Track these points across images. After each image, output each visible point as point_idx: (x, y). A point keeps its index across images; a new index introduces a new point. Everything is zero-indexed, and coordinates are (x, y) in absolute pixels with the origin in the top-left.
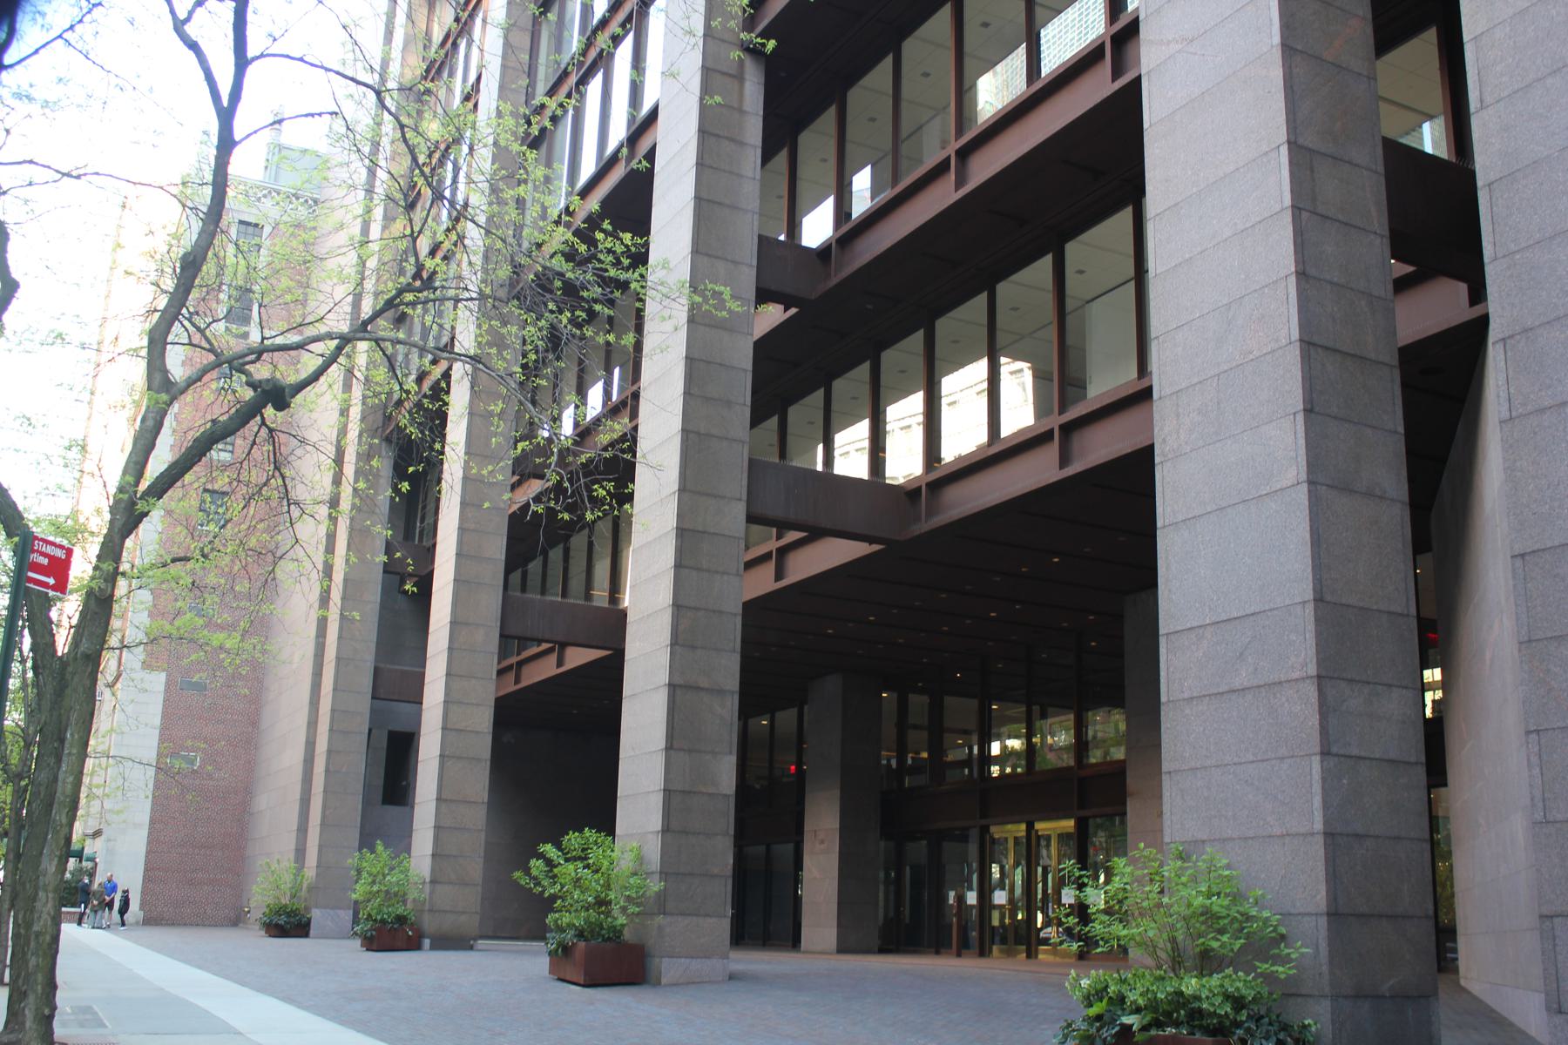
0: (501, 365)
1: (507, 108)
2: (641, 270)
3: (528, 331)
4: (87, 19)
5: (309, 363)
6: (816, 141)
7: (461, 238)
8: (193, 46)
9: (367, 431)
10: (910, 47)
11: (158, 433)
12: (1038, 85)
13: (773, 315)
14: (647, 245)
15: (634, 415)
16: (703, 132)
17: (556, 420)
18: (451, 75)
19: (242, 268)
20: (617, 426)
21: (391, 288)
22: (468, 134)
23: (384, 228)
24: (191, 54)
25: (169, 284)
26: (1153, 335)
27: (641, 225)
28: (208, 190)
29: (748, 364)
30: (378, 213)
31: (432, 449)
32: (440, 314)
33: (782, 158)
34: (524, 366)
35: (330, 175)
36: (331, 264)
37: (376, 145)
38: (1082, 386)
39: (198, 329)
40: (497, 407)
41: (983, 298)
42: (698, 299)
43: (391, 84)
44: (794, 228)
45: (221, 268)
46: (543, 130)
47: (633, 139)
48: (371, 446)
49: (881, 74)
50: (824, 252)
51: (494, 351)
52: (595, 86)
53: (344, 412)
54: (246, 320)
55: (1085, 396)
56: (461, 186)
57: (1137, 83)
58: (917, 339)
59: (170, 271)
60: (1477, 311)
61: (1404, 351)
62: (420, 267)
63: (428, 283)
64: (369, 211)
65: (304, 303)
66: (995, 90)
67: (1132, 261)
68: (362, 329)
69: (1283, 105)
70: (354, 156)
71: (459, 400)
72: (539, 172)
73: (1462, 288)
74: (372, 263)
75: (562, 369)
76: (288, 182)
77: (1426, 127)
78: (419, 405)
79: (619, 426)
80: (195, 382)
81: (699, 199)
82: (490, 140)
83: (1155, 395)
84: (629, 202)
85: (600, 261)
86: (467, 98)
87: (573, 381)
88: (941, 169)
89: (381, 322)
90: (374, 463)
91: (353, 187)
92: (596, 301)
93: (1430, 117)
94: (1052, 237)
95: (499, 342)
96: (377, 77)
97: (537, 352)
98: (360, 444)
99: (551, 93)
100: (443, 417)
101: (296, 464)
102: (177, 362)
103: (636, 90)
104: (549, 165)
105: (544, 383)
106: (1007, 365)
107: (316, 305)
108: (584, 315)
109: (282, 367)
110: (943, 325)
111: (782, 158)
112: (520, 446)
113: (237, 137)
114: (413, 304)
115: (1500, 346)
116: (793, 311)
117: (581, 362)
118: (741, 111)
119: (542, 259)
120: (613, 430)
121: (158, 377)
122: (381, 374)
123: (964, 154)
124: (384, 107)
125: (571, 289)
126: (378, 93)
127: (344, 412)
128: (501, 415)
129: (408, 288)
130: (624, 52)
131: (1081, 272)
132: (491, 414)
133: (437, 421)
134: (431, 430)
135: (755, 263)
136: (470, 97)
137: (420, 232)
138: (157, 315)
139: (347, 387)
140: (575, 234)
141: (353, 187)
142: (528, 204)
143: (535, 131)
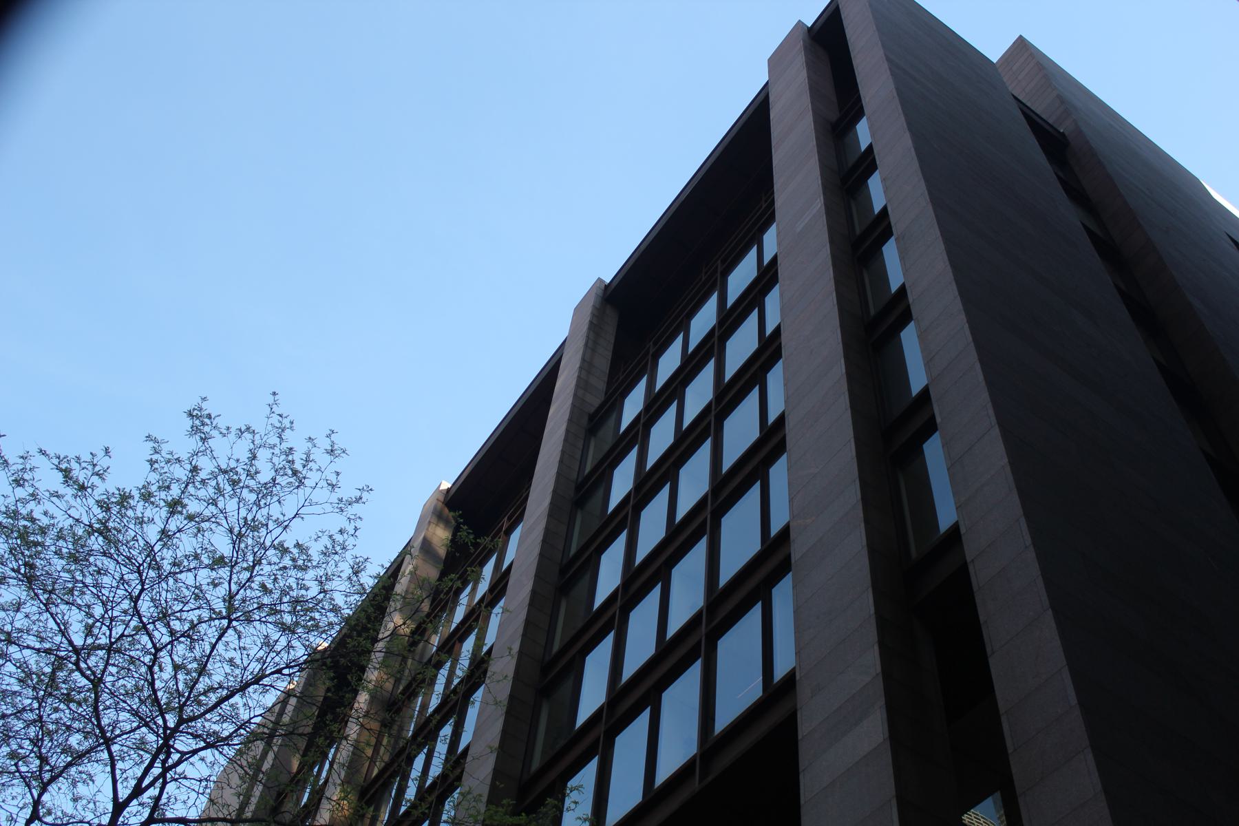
130: (447, 730)
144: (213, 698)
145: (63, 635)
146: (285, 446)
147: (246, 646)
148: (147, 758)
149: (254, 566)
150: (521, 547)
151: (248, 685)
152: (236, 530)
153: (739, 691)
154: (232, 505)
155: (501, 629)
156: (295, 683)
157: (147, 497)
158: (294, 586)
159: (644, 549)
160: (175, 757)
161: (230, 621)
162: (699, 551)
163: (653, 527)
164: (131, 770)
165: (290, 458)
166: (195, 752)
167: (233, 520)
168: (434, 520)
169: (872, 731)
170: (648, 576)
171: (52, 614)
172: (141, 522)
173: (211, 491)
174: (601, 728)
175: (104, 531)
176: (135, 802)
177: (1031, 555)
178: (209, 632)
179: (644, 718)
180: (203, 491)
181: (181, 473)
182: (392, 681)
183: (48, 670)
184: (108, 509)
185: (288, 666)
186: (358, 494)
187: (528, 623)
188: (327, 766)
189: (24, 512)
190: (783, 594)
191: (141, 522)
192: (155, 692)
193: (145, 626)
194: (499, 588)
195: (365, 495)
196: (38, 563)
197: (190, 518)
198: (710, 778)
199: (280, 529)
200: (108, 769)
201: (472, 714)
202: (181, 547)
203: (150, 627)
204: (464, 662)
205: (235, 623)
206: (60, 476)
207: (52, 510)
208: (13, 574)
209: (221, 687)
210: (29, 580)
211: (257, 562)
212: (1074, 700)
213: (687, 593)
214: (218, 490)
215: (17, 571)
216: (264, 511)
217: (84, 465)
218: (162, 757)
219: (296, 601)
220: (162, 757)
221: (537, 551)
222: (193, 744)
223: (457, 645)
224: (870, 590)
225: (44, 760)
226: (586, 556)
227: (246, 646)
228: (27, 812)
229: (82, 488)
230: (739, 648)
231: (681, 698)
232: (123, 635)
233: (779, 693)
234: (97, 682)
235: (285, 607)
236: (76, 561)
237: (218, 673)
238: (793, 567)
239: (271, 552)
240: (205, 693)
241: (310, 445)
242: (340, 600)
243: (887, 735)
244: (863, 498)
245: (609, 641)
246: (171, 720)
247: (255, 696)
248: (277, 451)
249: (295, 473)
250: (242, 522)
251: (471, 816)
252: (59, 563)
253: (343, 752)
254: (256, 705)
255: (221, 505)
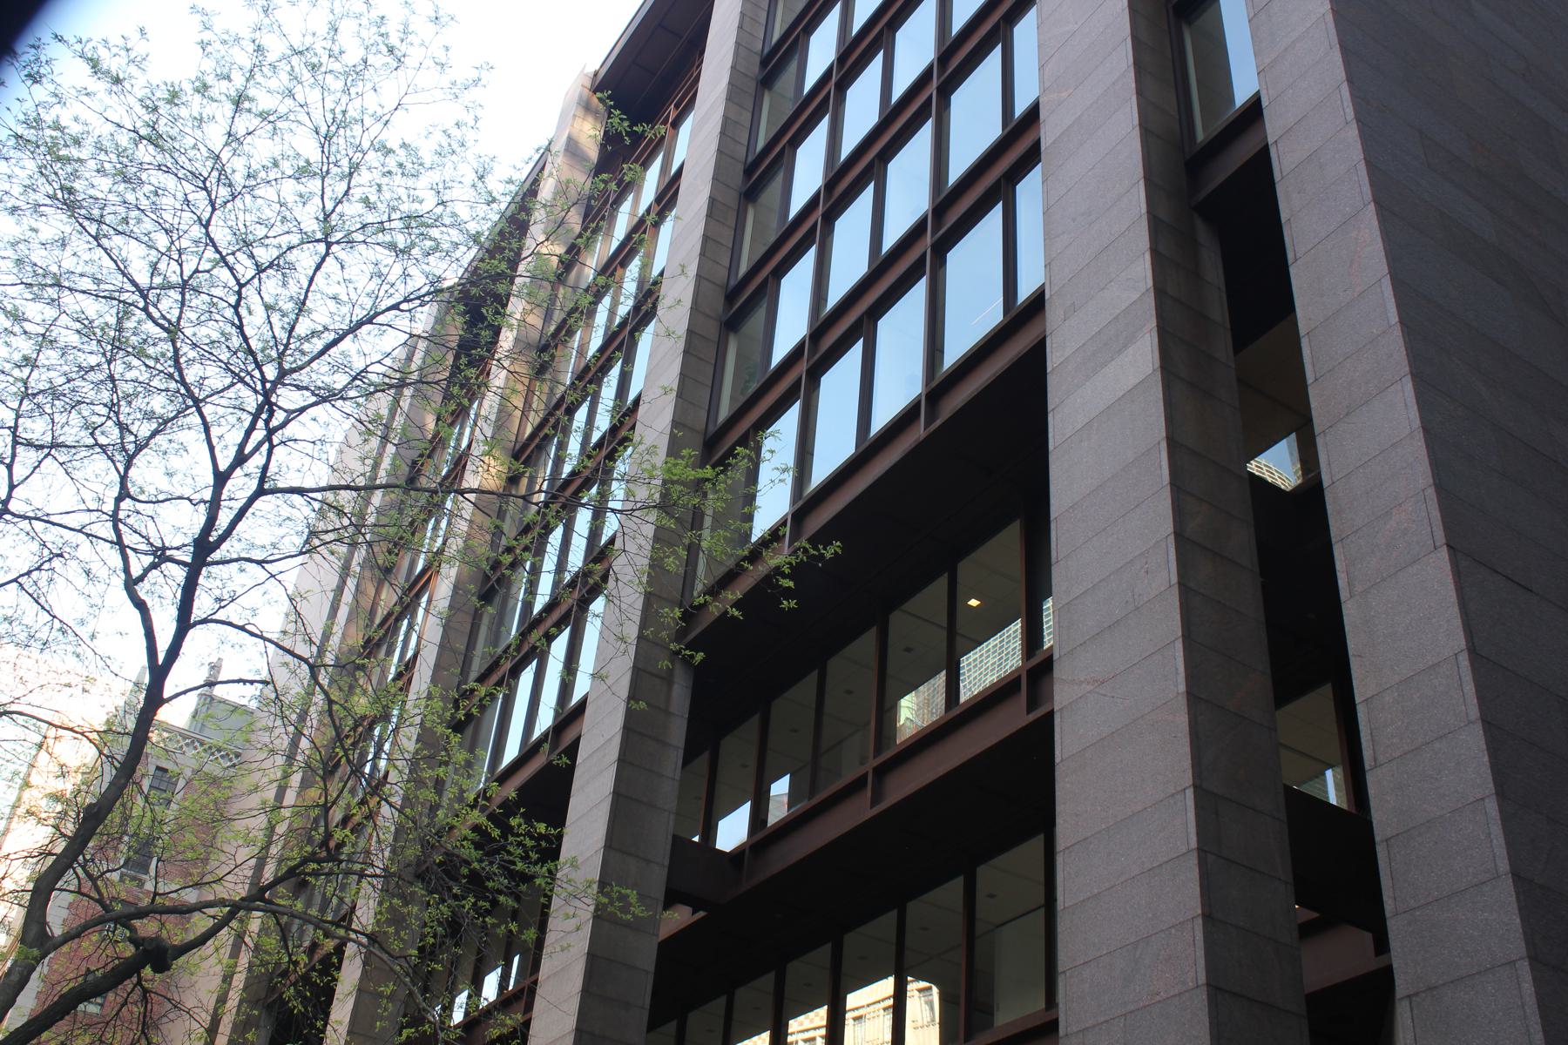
0: (396, 946)
1: (436, 691)
2: (551, 865)
3: (425, 913)
4: (46, 566)
5: (200, 923)
6: (738, 747)
7: (370, 816)
8: (141, 606)
9: (249, 999)
10: (835, 665)
11: (22, 988)
12: (956, 711)
13: (679, 917)
14: (560, 837)
15: (529, 1008)
16: (628, 729)
17: (448, 1008)
18: (390, 653)
19: (147, 821)
20: (508, 1022)
21: (295, 855)
22: (395, 712)
23: (299, 794)
24: (136, 614)
25: (70, 828)
26: (1060, 969)
27: (558, 817)
28: (127, 741)
29: (650, 966)
30: (296, 779)
31: (313, 1026)
32: (343, 887)
33: (703, 761)
34: (421, 950)
35: (253, 737)
36: (239, 825)
37: (303, 716)
38: (989, 1012)
39: (89, 876)
40: (387, 989)
41: (893, 915)
42: (606, 900)
43: (329, 659)
44: (710, 832)
45: (126, 818)
46: (469, 716)
47: (559, 727)
48: (249, 1016)
49: (805, 690)
50: (739, 853)
51: (392, 930)
52: (527, 678)
53: (227, 979)
54: (145, 869)
55: (990, 1024)
56: (382, 764)
57: (1049, 717)
58: (824, 953)
59: (73, 814)
60: (1379, 963)
61: (1307, 996)
62: (329, 835)
63: (334, 857)
64: (286, 776)
65: (206, 861)
66: (914, 711)
67: (1042, 888)
68: (258, 896)
69: (1188, 749)
70: (279, 722)
71: (350, 975)
72: (460, 756)
73: (1368, 936)
74: (281, 829)
75: (458, 957)
76: (215, 737)
77: (1329, 774)
78: (305, 978)
79: (511, 1020)
80: (72, 938)
81: (618, 795)
82: (418, 720)
83: (1062, 1032)
84: (545, 787)
85: (509, 853)
86: (399, 676)
87: (470, 973)
88: (858, 785)
89: (281, 889)
90: (249, 1036)
91: (273, 752)
92: (500, 892)
93: (1331, 766)
94: (966, 863)
95: (397, 920)
96: (315, 649)
97: (435, 936)
98: (238, 1014)
99: (481, 679)
100: (329, 993)
101: (164, 1028)
102: (58, 915)
103: (566, 688)
104: (472, 750)
105: (439, 967)
106: (914, 987)
107: (219, 865)
108: (487, 905)
109: (168, 926)
110: (851, 940)
111: (703, 761)
112: (405, 1033)
113: (166, 695)
114: (316, 874)
115: (1406, 1003)
116: (701, 914)
117: (479, 951)
118: (667, 713)
119: (450, 843)
120: (503, 1025)
121: (34, 930)
122: (272, 942)
123: (882, 771)
124: (317, 683)
125: (477, 881)
126: (312, 668)
127: (227, 979)
128: (390, 998)
129: (312, 858)
130: (559, 647)
131: (991, 896)
132: (381, 995)
133: (324, 998)
134: (314, 1006)
135: (667, 862)
136: (408, 667)
137: (334, 803)
138: (51, 859)
139: (235, 954)
140: (491, 817)
141: (273, 752)
142: (447, 785)
143: (461, 715)
144: (318, 344)
145: (124, 274)
146: (374, 14)
147: (352, 278)
148: (248, 419)
149: (351, 174)
150: (695, 142)
151: (360, 324)
152: (323, 130)
153: (973, 313)
154: (314, 96)
155: (675, 249)
156: (424, 319)
157: (203, 89)
158: (405, 198)
159: (851, 140)
160: (279, 417)
161: (329, 245)
162: (924, 137)
163: (862, 109)
164: (229, 439)
165: (383, 30)
166: (302, 410)
167: (317, 116)
168: (580, 113)
169: (1141, 358)
170: (857, 174)
171: (105, 250)
172: (200, 121)
173: (284, 77)
174: (802, 367)
175: (155, 140)
176: (238, 472)
177: (1353, 132)
178: (305, 259)
179: (856, 352)
180: (274, 80)
181: (244, 59)
182: (540, 312)
183: (113, 321)
184: (155, 109)
185: (406, 300)
186: (474, 74)
187: (706, 238)
188: (468, 431)
189: (49, 118)
190: (1029, 191)
191: (200, 121)
192: (246, 339)
193: (223, 258)
194: (667, 197)
195: (485, 75)
196: (77, 185)
197: (264, 116)
198: (938, 422)
199: (380, 125)
200: (203, 436)
201: (592, 633)
202: (256, 157)
203: (230, 259)
204: (630, 287)
205: (335, 248)
206: (86, 69)
207: (86, 115)
208: (48, 201)
209: (326, 329)
210: (70, 203)
211: (354, 168)
212: (1394, 317)
213: (908, 190)
214: (294, 77)
215: (53, 197)
216: (357, 103)
217: (115, 50)
218: (264, 416)
219: (408, 218)
220: (264, 416)
221: (714, 146)
222: (306, 398)
223: (619, 272)
224: (1142, 183)
225: (124, 428)
226: (777, 149)
227: (352, 278)
228: (115, 492)
229: (117, 81)
230: (973, 264)
231: (902, 328)
232: (197, 271)
233: (1025, 315)
234: (173, 331)
235: (397, 224)
236: (126, 180)
237: (322, 314)
238: (1043, 156)
239: (371, 155)
240: (307, 338)
241: (407, 11)
242: (464, 213)
243: (1157, 364)
244: (1136, 63)
245: (809, 258)
246: (271, 372)
247: (370, 338)
248: (364, 21)
249: (391, 50)
250: (329, 117)
251: (644, 471)
252: (104, 183)
253: (489, 404)
254: (378, 349)
255: (300, 98)
